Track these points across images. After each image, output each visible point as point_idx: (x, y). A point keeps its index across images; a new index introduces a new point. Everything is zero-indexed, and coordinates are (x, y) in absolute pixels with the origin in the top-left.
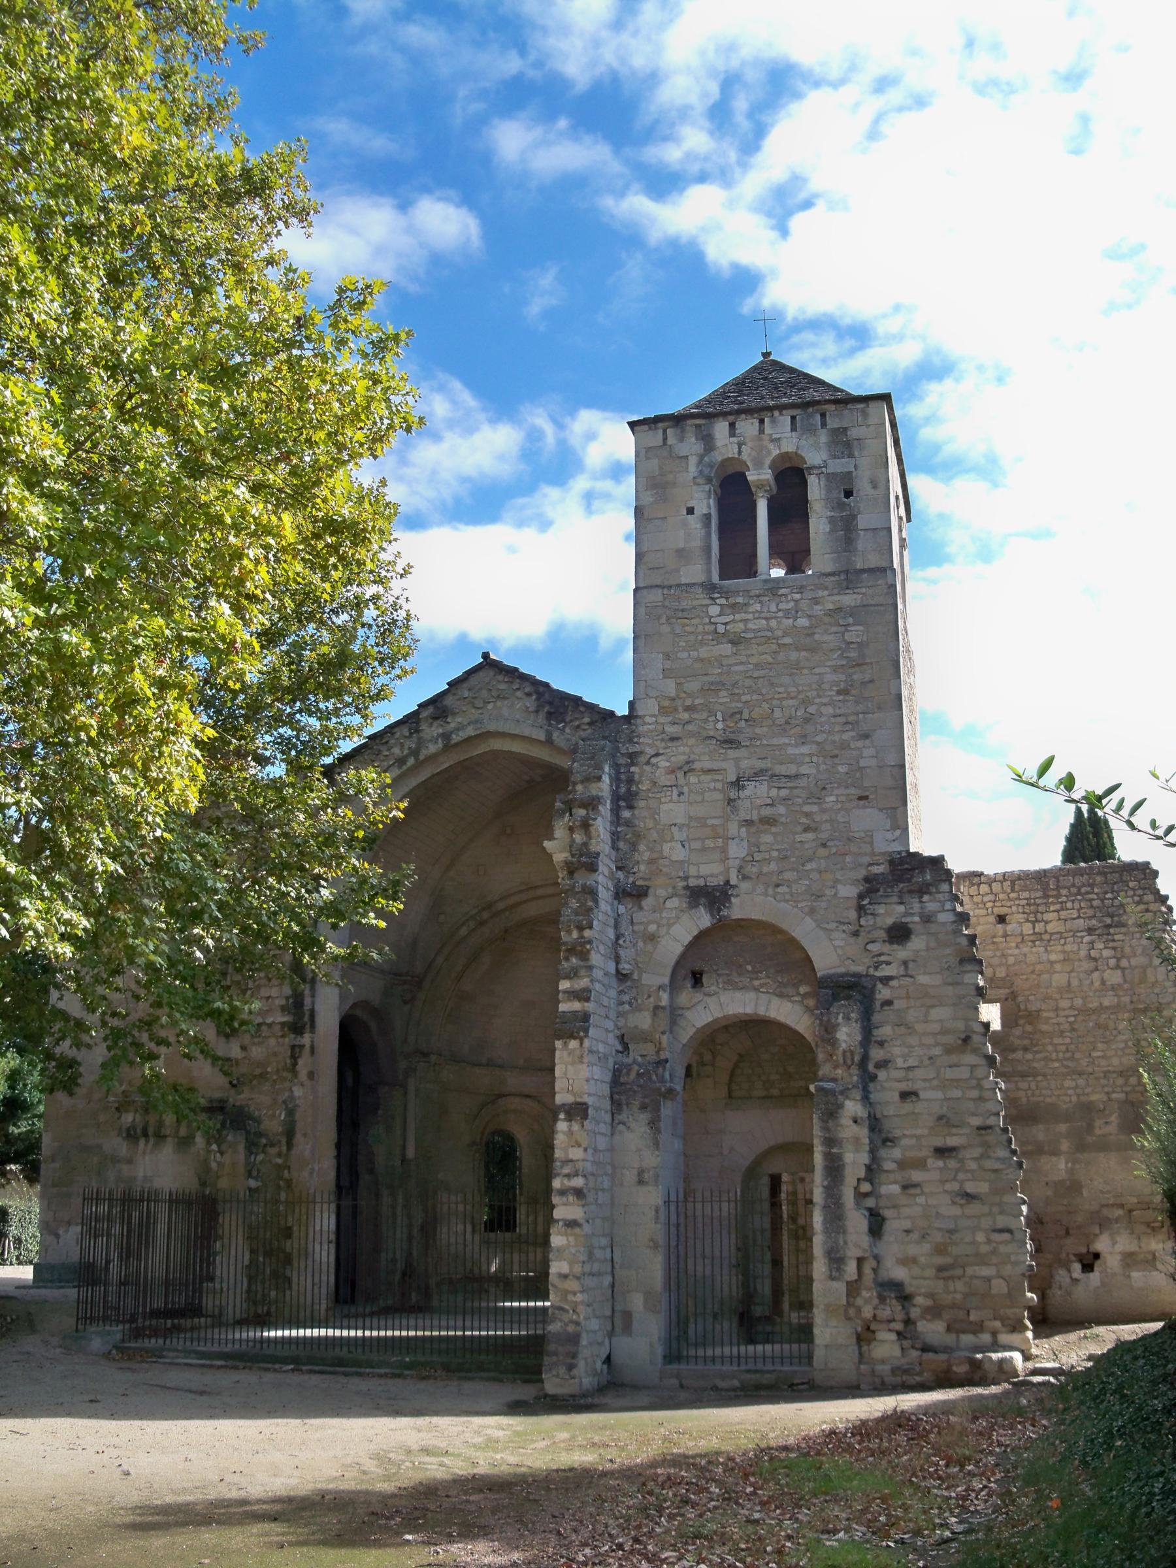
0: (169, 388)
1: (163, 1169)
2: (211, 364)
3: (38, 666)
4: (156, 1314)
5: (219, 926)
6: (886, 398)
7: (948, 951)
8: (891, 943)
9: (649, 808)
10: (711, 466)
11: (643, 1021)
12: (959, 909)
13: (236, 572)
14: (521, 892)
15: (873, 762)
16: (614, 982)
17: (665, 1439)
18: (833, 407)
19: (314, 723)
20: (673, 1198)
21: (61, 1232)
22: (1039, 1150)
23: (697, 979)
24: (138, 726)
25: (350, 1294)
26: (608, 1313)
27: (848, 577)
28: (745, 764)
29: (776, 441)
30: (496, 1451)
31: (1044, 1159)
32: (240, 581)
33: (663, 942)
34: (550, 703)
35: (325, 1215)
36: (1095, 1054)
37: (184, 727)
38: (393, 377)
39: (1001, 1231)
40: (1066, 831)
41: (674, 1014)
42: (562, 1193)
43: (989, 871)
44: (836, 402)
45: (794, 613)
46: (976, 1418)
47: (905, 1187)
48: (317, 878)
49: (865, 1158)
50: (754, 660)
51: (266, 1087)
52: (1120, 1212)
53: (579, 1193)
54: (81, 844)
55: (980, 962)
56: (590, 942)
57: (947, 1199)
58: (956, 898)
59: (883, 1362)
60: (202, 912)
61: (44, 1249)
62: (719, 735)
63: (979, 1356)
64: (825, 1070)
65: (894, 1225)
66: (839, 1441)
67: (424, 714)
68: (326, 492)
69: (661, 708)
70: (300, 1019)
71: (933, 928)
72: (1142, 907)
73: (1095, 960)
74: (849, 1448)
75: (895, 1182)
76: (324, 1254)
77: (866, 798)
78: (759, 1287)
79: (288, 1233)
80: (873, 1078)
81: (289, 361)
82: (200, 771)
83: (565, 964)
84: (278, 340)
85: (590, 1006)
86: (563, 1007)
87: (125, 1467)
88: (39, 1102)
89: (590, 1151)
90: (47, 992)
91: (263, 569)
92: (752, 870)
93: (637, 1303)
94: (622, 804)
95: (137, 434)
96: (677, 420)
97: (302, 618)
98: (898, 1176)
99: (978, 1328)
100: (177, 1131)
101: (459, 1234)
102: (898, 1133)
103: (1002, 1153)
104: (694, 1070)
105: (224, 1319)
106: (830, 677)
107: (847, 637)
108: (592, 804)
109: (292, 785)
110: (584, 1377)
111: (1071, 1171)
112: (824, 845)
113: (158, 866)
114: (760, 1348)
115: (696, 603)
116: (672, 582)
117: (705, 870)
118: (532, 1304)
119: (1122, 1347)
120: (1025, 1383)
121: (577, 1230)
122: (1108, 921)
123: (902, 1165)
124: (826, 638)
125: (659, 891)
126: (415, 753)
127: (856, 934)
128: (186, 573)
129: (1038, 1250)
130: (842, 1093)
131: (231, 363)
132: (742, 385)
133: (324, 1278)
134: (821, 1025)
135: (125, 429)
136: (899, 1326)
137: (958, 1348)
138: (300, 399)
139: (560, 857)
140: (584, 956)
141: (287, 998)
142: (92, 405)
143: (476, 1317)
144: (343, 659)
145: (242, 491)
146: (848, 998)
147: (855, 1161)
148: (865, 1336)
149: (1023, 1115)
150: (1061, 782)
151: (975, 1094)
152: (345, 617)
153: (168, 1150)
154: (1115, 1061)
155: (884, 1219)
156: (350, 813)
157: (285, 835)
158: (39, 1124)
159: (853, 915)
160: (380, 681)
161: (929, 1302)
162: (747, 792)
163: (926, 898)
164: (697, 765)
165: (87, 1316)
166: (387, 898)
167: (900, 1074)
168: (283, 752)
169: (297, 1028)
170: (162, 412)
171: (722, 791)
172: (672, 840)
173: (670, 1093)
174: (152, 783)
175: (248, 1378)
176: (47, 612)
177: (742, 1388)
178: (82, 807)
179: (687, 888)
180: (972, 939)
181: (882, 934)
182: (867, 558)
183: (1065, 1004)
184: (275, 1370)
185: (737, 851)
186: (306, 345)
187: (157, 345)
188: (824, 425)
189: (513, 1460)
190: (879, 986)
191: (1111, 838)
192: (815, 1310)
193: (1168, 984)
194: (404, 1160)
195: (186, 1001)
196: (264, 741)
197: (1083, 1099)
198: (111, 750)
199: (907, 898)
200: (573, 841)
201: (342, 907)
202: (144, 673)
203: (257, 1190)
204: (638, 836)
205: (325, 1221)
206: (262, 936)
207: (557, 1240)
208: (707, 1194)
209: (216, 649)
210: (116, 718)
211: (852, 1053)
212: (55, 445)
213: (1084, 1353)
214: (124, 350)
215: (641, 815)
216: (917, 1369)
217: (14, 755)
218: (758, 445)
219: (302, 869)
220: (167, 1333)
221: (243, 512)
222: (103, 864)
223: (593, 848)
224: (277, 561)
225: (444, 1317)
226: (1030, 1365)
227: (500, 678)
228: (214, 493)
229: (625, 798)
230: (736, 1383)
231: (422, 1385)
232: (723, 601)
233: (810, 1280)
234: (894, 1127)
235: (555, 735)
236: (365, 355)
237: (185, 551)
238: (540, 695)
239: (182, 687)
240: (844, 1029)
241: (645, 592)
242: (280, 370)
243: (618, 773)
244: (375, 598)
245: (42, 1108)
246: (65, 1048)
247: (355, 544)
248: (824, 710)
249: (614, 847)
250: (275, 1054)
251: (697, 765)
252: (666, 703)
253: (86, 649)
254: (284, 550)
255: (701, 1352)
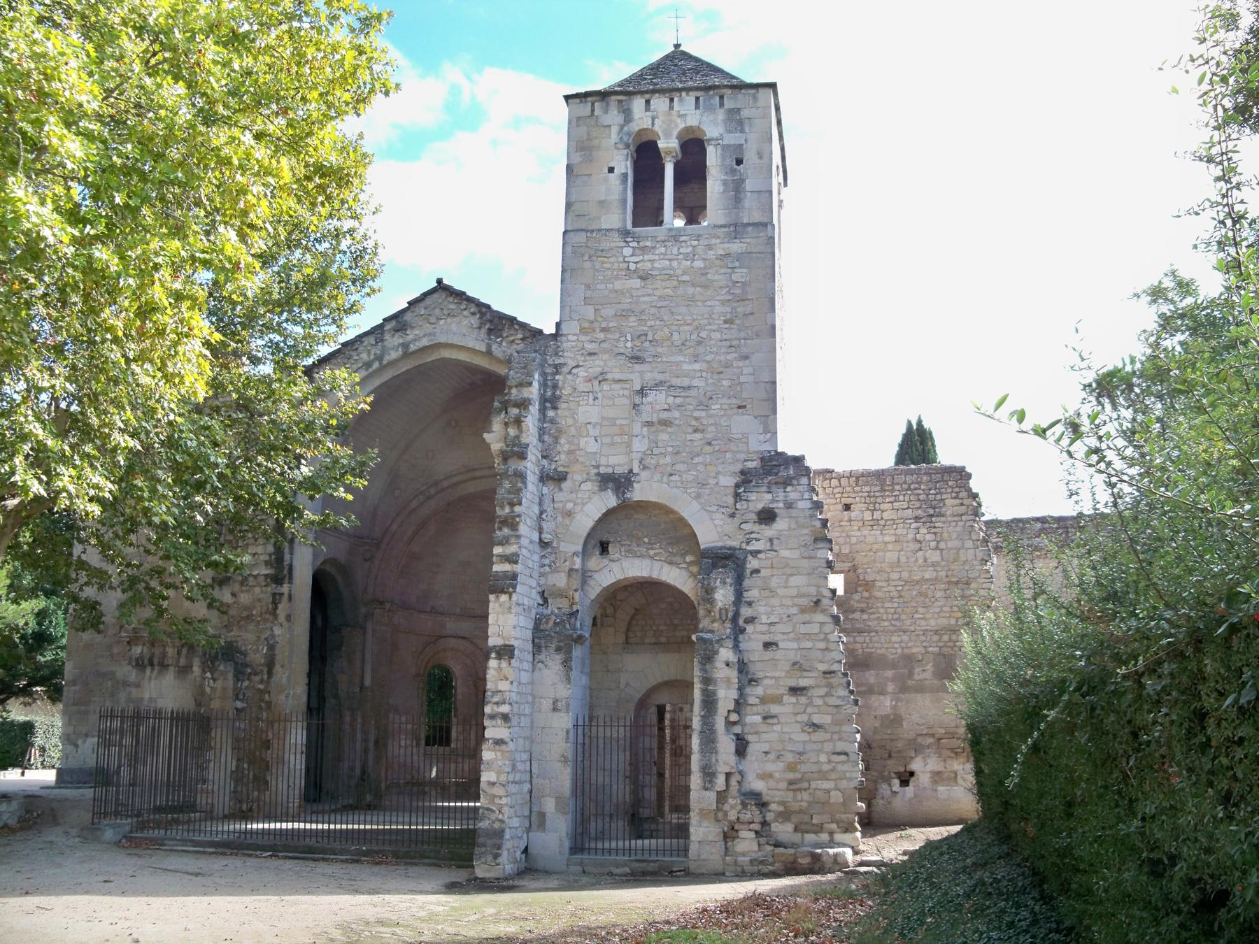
0: (189, 49)
1: (166, 692)
2: (224, 31)
3: (73, 277)
4: (159, 809)
5: (216, 495)
6: (773, 86)
7: (805, 531)
8: (760, 524)
9: (569, 409)
10: (629, 134)
11: (560, 580)
12: (815, 498)
13: (242, 205)
14: (461, 473)
15: (751, 379)
16: (537, 549)
17: (573, 914)
18: (730, 91)
19: (298, 330)
20: (581, 722)
21: (80, 742)
22: (870, 691)
23: (604, 548)
24: (157, 329)
25: (316, 794)
26: (527, 813)
27: (736, 229)
28: (648, 376)
29: (683, 116)
30: (437, 923)
31: (874, 698)
32: (245, 213)
33: (578, 517)
34: (491, 321)
35: (299, 731)
36: (916, 616)
37: (196, 331)
38: (376, 49)
39: (839, 754)
40: (899, 439)
41: (585, 576)
42: (492, 717)
43: (839, 469)
44: (733, 87)
45: (692, 256)
46: (817, 900)
47: (765, 718)
48: (298, 458)
49: (734, 694)
50: (658, 293)
51: (251, 627)
52: (931, 740)
53: (505, 717)
54: (105, 425)
55: (830, 541)
56: (519, 516)
57: (798, 728)
58: (813, 490)
59: (744, 855)
60: (206, 482)
61: (65, 757)
62: (628, 352)
63: (819, 851)
64: (704, 623)
65: (754, 749)
66: (710, 917)
67: (387, 327)
68: (317, 142)
69: (582, 329)
70: (280, 572)
71: (794, 512)
72: (958, 501)
73: (920, 542)
74: (718, 923)
75: (758, 714)
76: (296, 762)
77: (744, 407)
78: (647, 795)
79: (267, 745)
80: (743, 631)
81: (289, 31)
82: (207, 366)
83: (498, 533)
84: (281, 13)
85: (518, 568)
86: (496, 568)
87: (135, 936)
88: (63, 636)
89: (515, 684)
90: (71, 546)
91: (264, 203)
92: (650, 461)
93: (549, 805)
94: (548, 405)
95: (159, 86)
96: (603, 95)
97: (290, 245)
98: (760, 709)
99: (819, 829)
100: (178, 661)
101: (404, 748)
102: (760, 675)
103: (843, 692)
104: (599, 621)
105: (215, 814)
106: (719, 309)
107: (734, 277)
108: (523, 404)
109: (280, 380)
110: (506, 864)
111: (894, 708)
112: (709, 444)
113: (171, 443)
114: (647, 842)
115: (613, 245)
116: (594, 227)
117: (613, 460)
118: (465, 804)
119: (930, 845)
120: (854, 873)
121: (504, 747)
122: (931, 511)
123: (763, 700)
124: (717, 277)
125: (576, 476)
126: (379, 358)
127: (732, 516)
128: (198, 203)
129: (867, 769)
130: (718, 642)
131: (241, 30)
132: (656, 69)
133: (297, 782)
134: (702, 587)
135: (148, 81)
136: (757, 827)
137: (803, 845)
138: (298, 64)
139: (496, 446)
140: (514, 526)
141: (270, 555)
142: (119, 59)
143: (420, 814)
144: (323, 280)
145: (248, 138)
146: (724, 566)
147: (726, 696)
148: (730, 835)
149: (858, 663)
150: (1012, 414)
151: (822, 645)
152: (327, 245)
153: (169, 678)
154: (933, 622)
155: (748, 743)
156: (325, 405)
157: (273, 422)
158: (62, 654)
159: (731, 500)
160: (353, 298)
161: (781, 809)
162: (649, 399)
163: (789, 489)
164: (609, 376)
165: (102, 811)
166: (354, 476)
167: (764, 628)
168: (273, 354)
169: (277, 580)
170: (180, 68)
171: (629, 397)
172: (588, 435)
173: (579, 639)
174: (168, 378)
175: (235, 862)
176: (81, 232)
177: (632, 874)
178: (107, 394)
179: (598, 474)
180: (824, 523)
181: (755, 517)
182: (750, 213)
183: (895, 576)
184: (257, 856)
185: (639, 446)
186: (305, 19)
187: (178, 11)
188: (722, 105)
189: (451, 930)
190: (750, 557)
191: (933, 445)
192: (691, 814)
193: (975, 563)
194: (362, 687)
195: (189, 554)
196: (257, 344)
197: (906, 651)
198: (133, 349)
199: (774, 488)
200: (507, 434)
201: (319, 482)
202: (162, 286)
203: (243, 709)
204: (559, 431)
205: (297, 736)
206: (253, 501)
207: (487, 755)
208: (608, 719)
209: (223, 268)
210: (139, 323)
211: (727, 611)
212: (91, 92)
213: (900, 849)
214: (150, 14)
215: (563, 414)
216: (771, 860)
217: (49, 351)
218: (667, 121)
219: (286, 450)
220: (168, 825)
221: (248, 156)
222: (125, 441)
223: (524, 440)
224: (273, 196)
225: (394, 814)
226: (858, 858)
227: (451, 299)
228: (223, 139)
229: (550, 401)
230: (627, 870)
231: (376, 869)
232: (635, 244)
233: (687, 789)
234: (757, 670)
235: (494, 347)
236: (353, 30)
237: (199, 186)
238: (483, 315)
239: (193, 299)
240: (721, 591)
241: (572, 234)
242: (281, 39)
243: (545, 380)
244: (351, 231)
245: (64, 641)
246: (90, 592)
247: (339, 186)
248: (714, 335)
249: (541, 440)
250: (259, 600)
251: (609, 376)
252: (586, 325)
253: (115, 265)
254: (281, 188)
255: (600, 845)
